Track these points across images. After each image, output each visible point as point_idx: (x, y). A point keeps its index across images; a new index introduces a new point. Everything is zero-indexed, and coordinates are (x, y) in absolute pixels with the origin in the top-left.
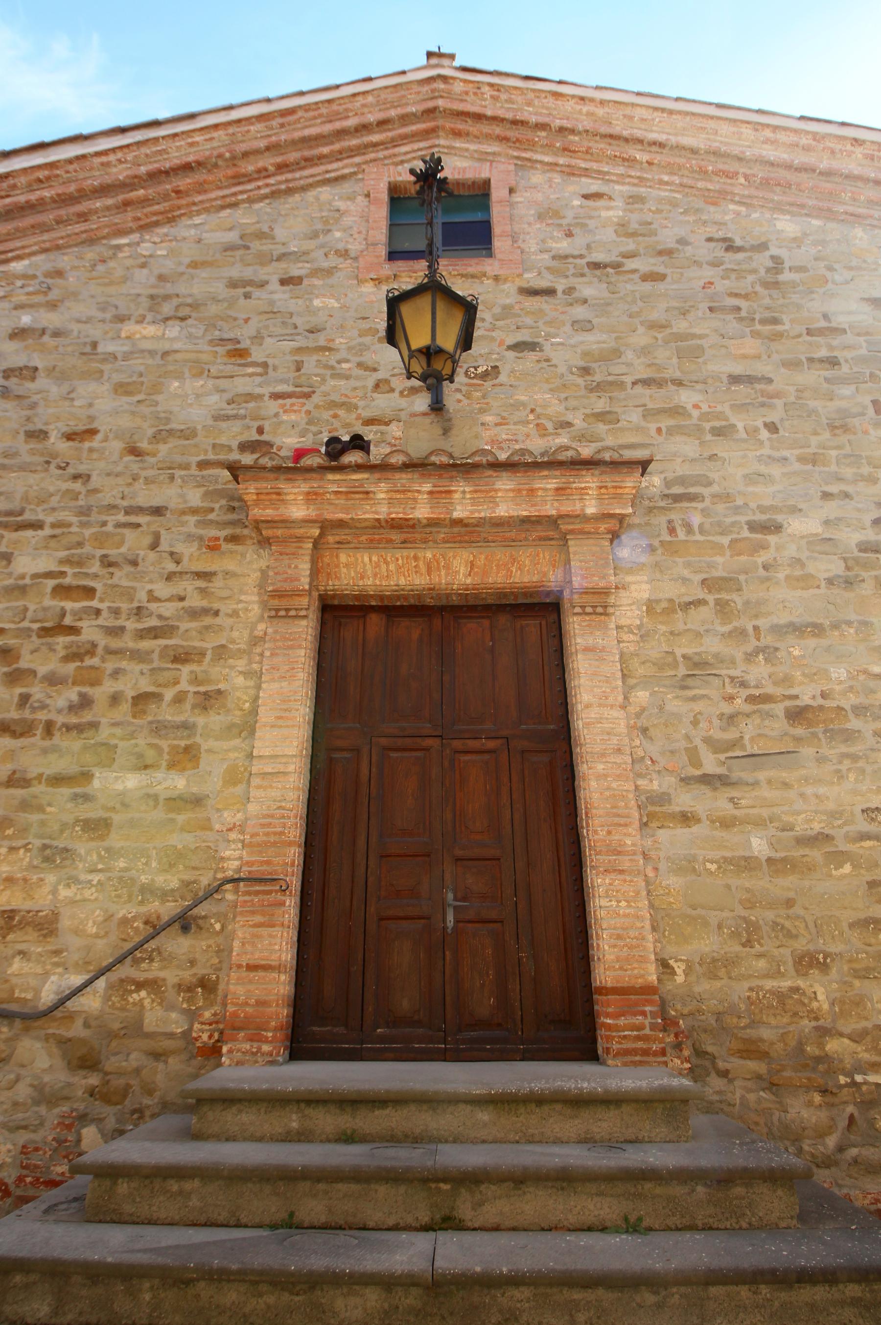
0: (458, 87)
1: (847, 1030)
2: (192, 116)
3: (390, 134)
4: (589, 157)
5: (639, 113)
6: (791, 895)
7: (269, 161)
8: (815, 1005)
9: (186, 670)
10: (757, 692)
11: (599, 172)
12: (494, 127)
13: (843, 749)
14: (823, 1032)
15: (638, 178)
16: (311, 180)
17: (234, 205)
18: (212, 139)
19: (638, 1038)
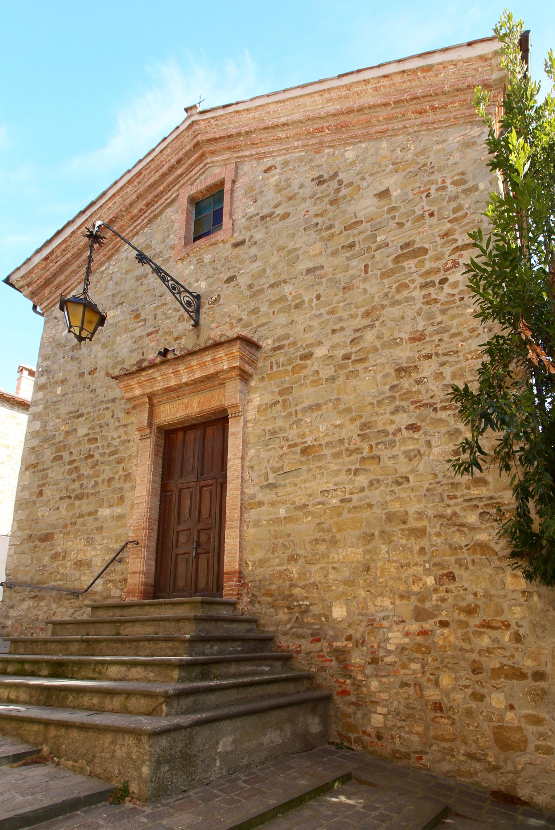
0: (202, 125)
1: (300, 585)
2: (104, 194)
3: (185, 166)
4: (263, 144)
5: (273, 107)
6: (289, 532)
7: (141, 204)
8: (292, 575)
9: (121, 466)
10: (291, 443)
12: (223, 143)
13: (318, 464)
14: (292, 586)
15: (285, 149)
16: (161, 207)
17: (137, 233)
18: (115, 202)
19: (231, 590)
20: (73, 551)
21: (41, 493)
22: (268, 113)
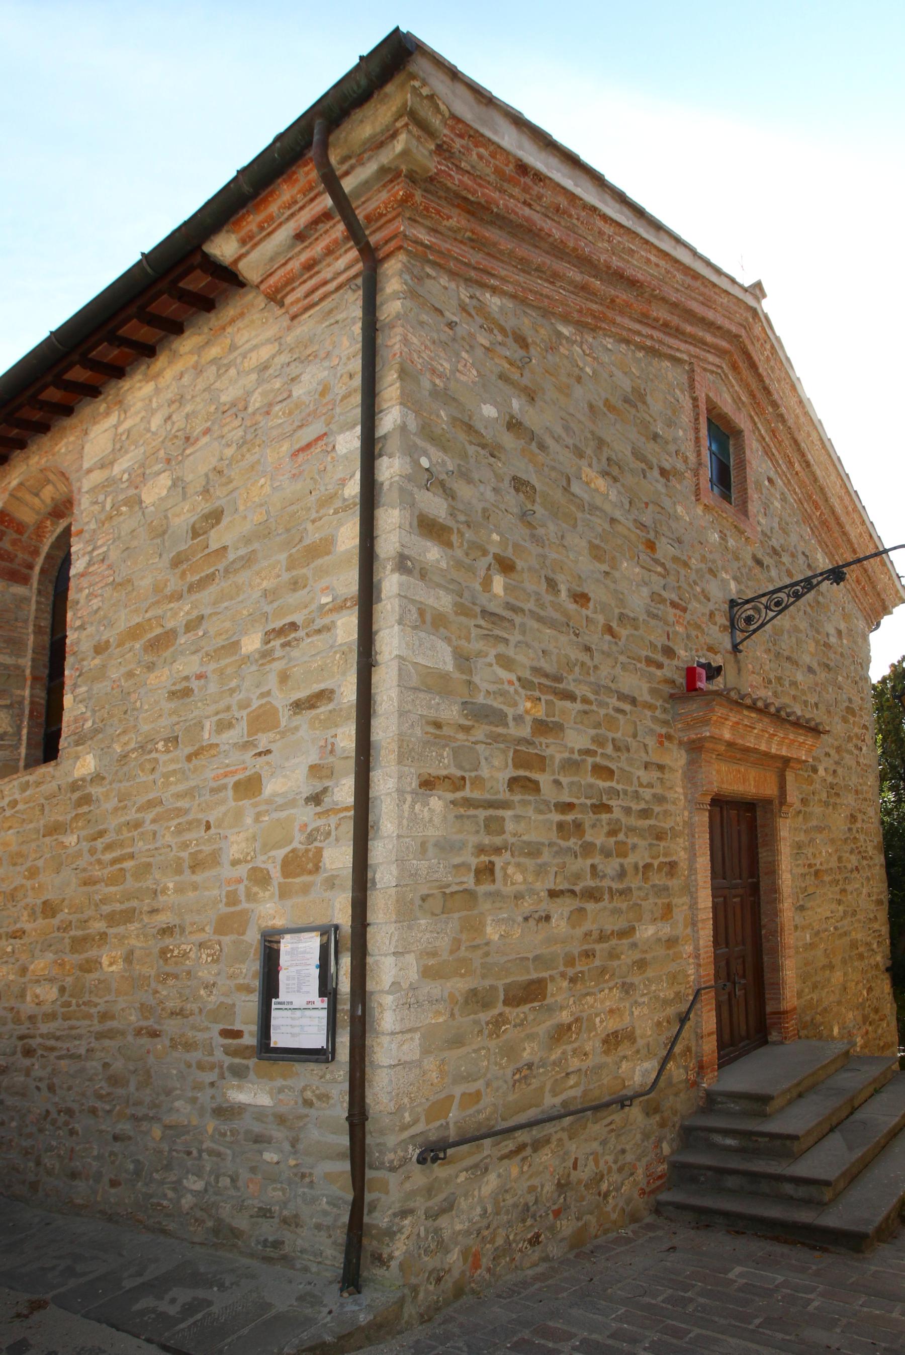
11: (777, 461)
17: (627, 342)
20: (597, 1015)
21: (486, 872)
22: (809, 435)
